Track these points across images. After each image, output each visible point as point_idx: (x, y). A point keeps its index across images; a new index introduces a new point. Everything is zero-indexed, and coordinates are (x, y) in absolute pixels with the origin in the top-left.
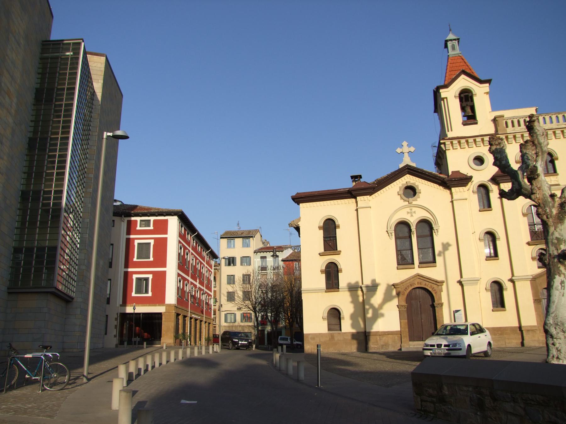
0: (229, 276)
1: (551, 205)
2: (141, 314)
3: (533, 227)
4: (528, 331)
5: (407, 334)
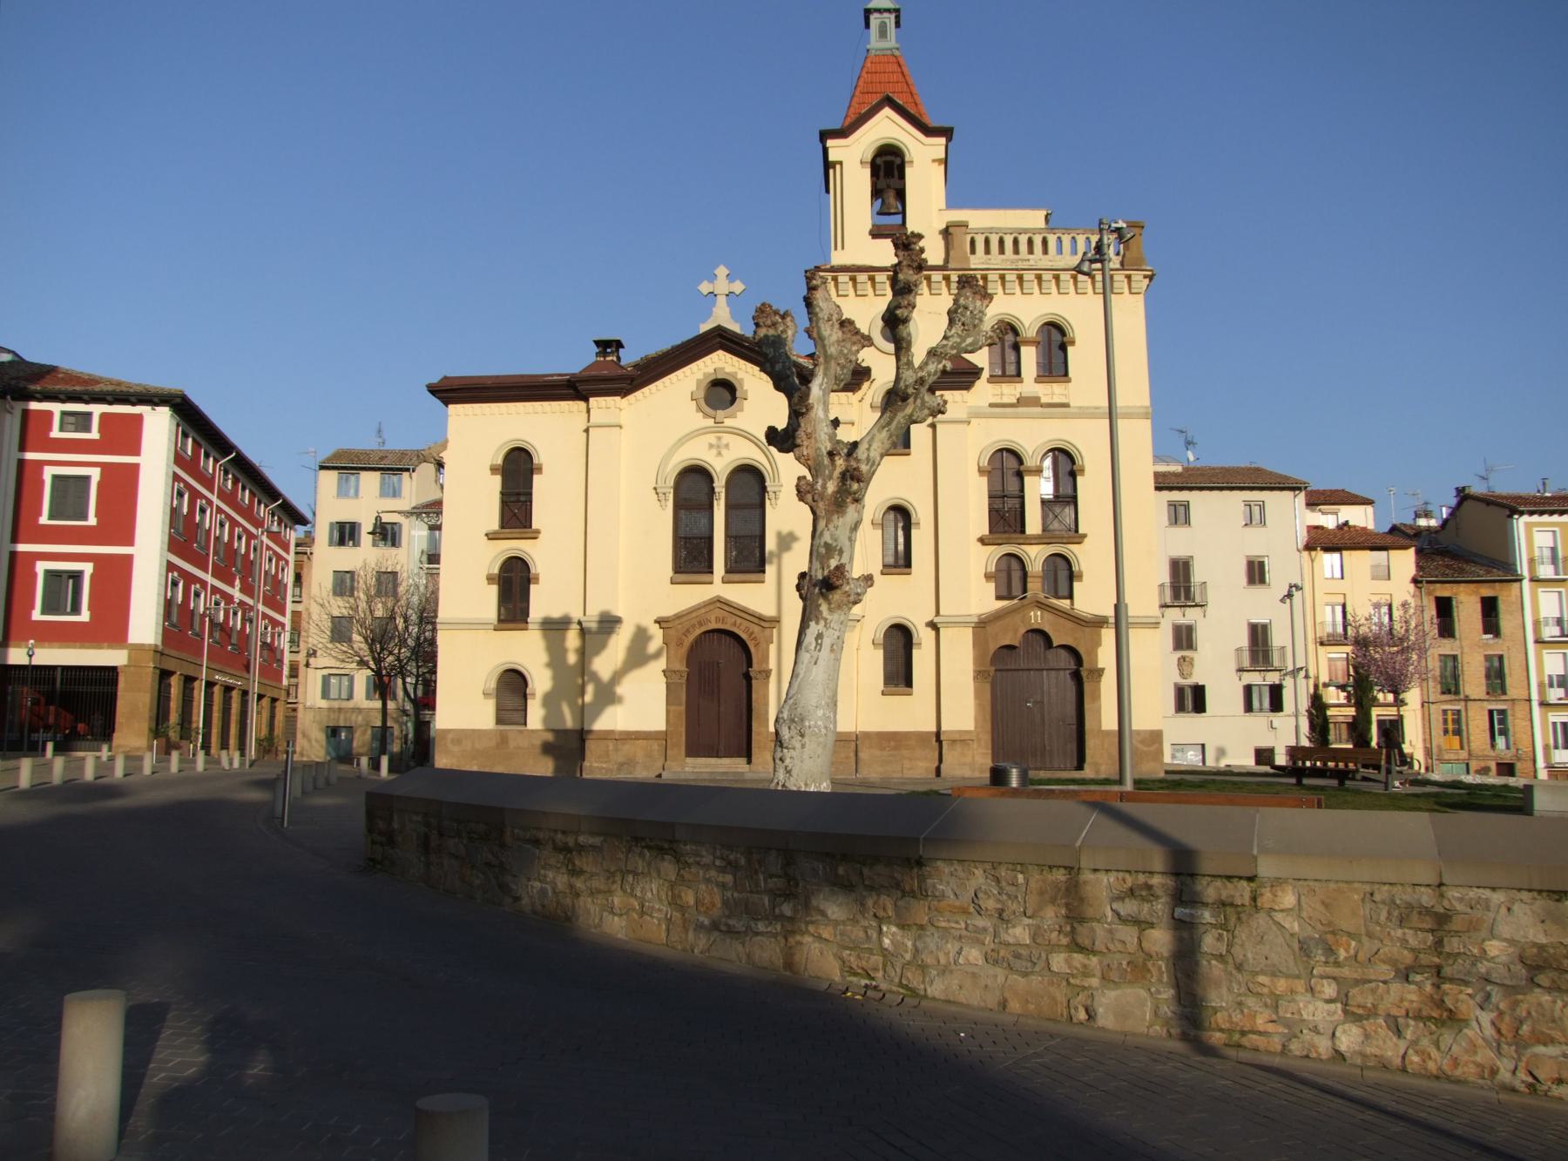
0: (340, 574)
1: (827, 472)
2: (59, 669)
3: (998, 501)
4: (954, 741)
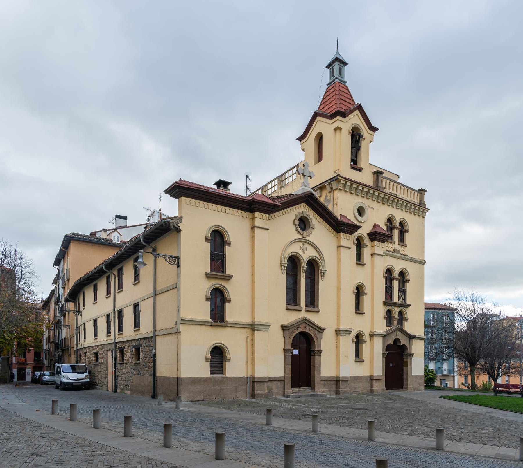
5: (289, 381)
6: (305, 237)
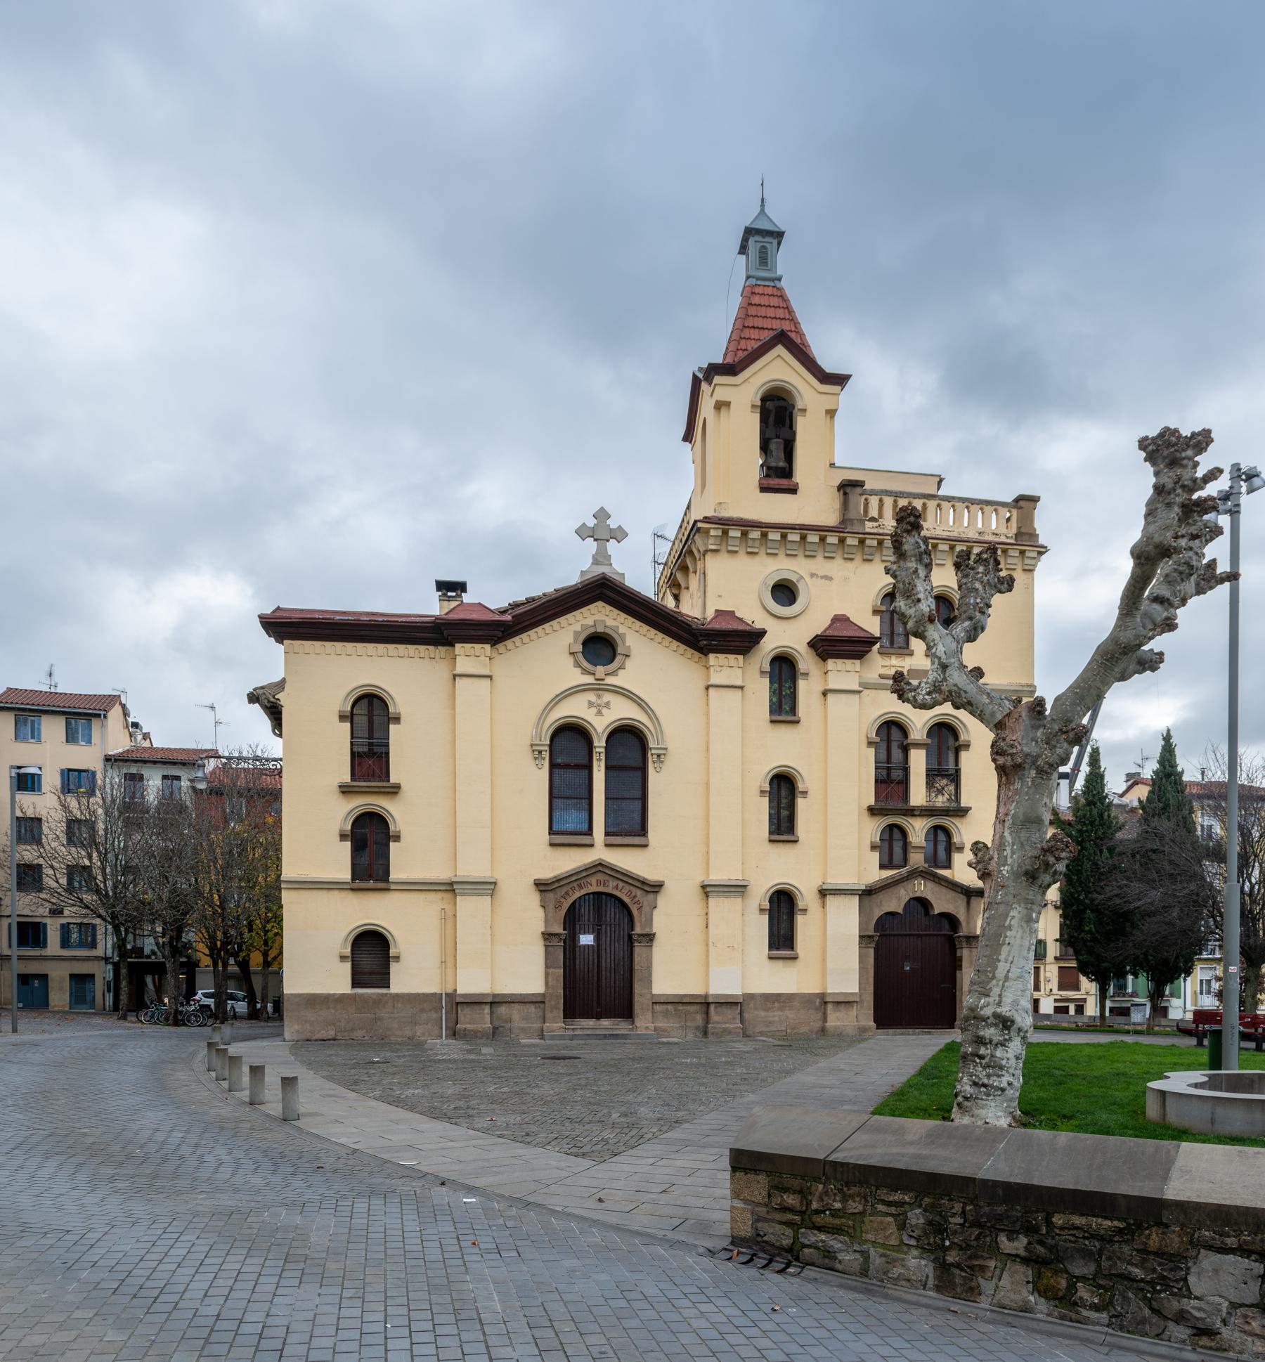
6: (603, 680)
